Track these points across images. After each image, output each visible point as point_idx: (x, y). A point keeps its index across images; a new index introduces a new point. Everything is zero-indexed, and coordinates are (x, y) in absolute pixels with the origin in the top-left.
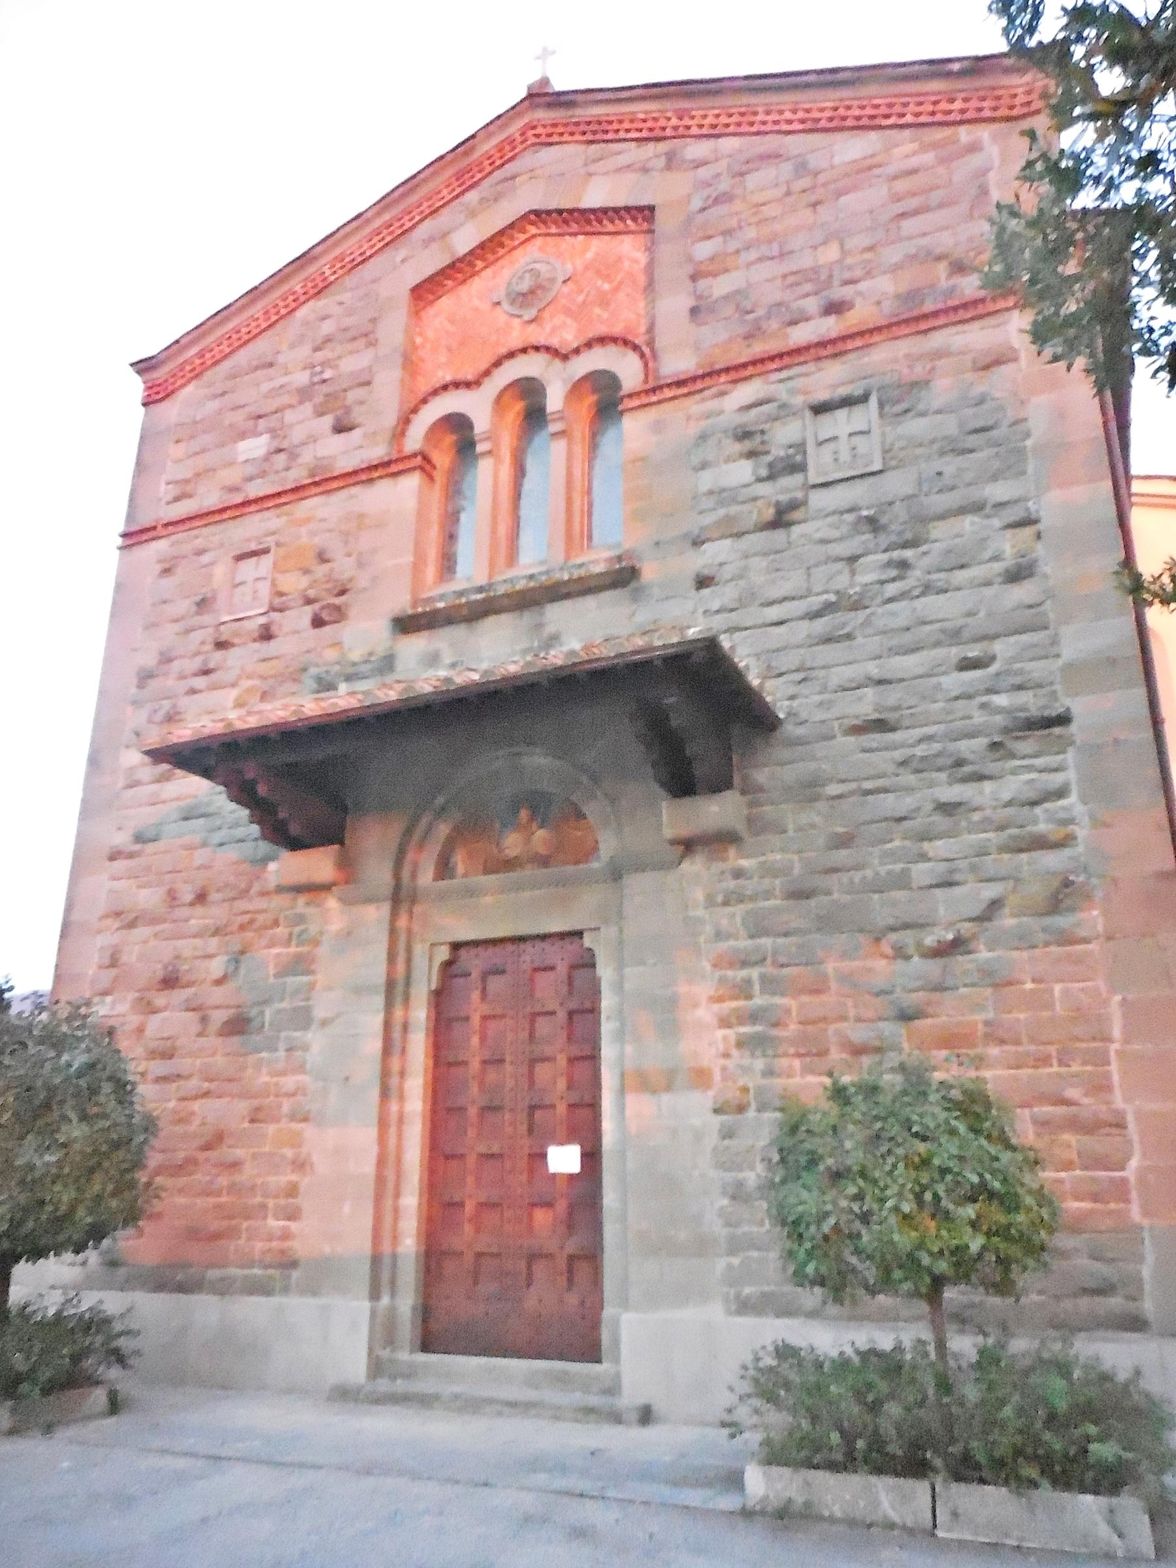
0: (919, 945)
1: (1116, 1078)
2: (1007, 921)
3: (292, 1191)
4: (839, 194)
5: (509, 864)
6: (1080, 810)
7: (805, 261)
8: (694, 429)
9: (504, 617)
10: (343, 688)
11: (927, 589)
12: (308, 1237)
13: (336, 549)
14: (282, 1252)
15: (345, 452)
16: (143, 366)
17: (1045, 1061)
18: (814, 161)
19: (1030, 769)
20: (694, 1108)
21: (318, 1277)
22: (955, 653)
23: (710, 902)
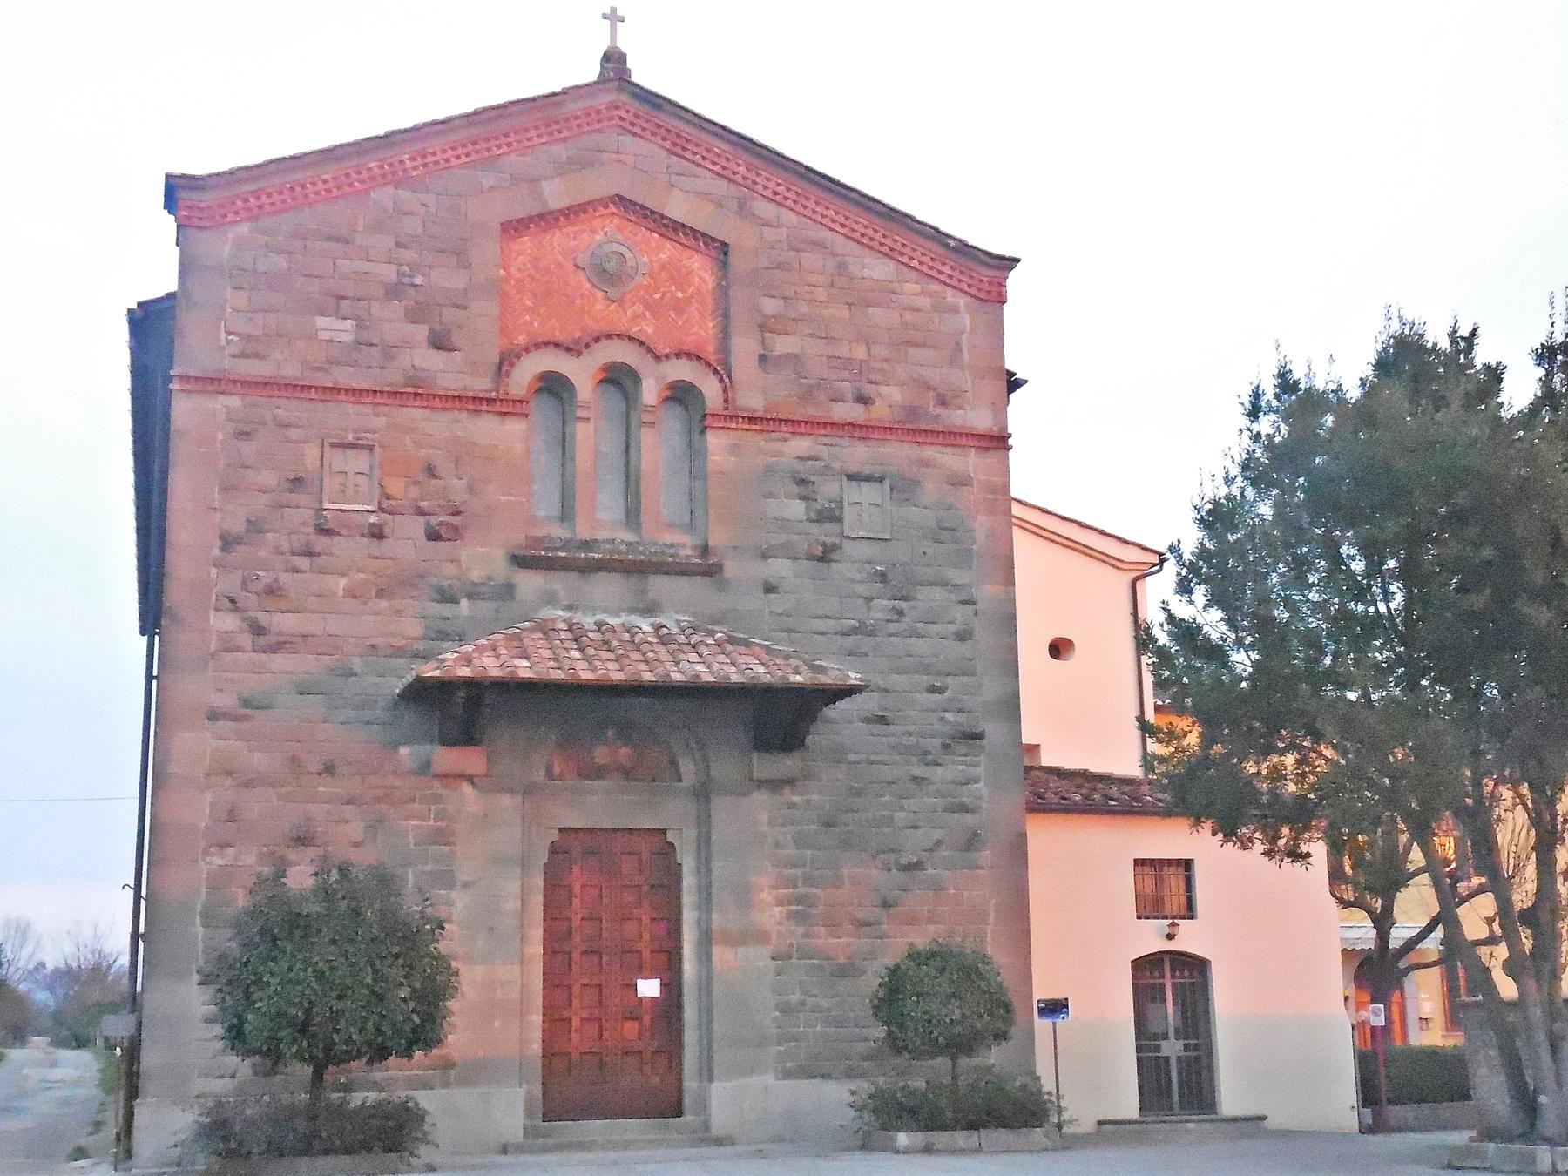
0: (897, 863)
5: (598, 773)
6: (985, 792)
7: (844, 351)
10: (464, 602)
13: (443, 465)
14: (441, 1057)
19: (962, 763)
20: (758, 957)
22: (925, 680)
23: (771, 823)
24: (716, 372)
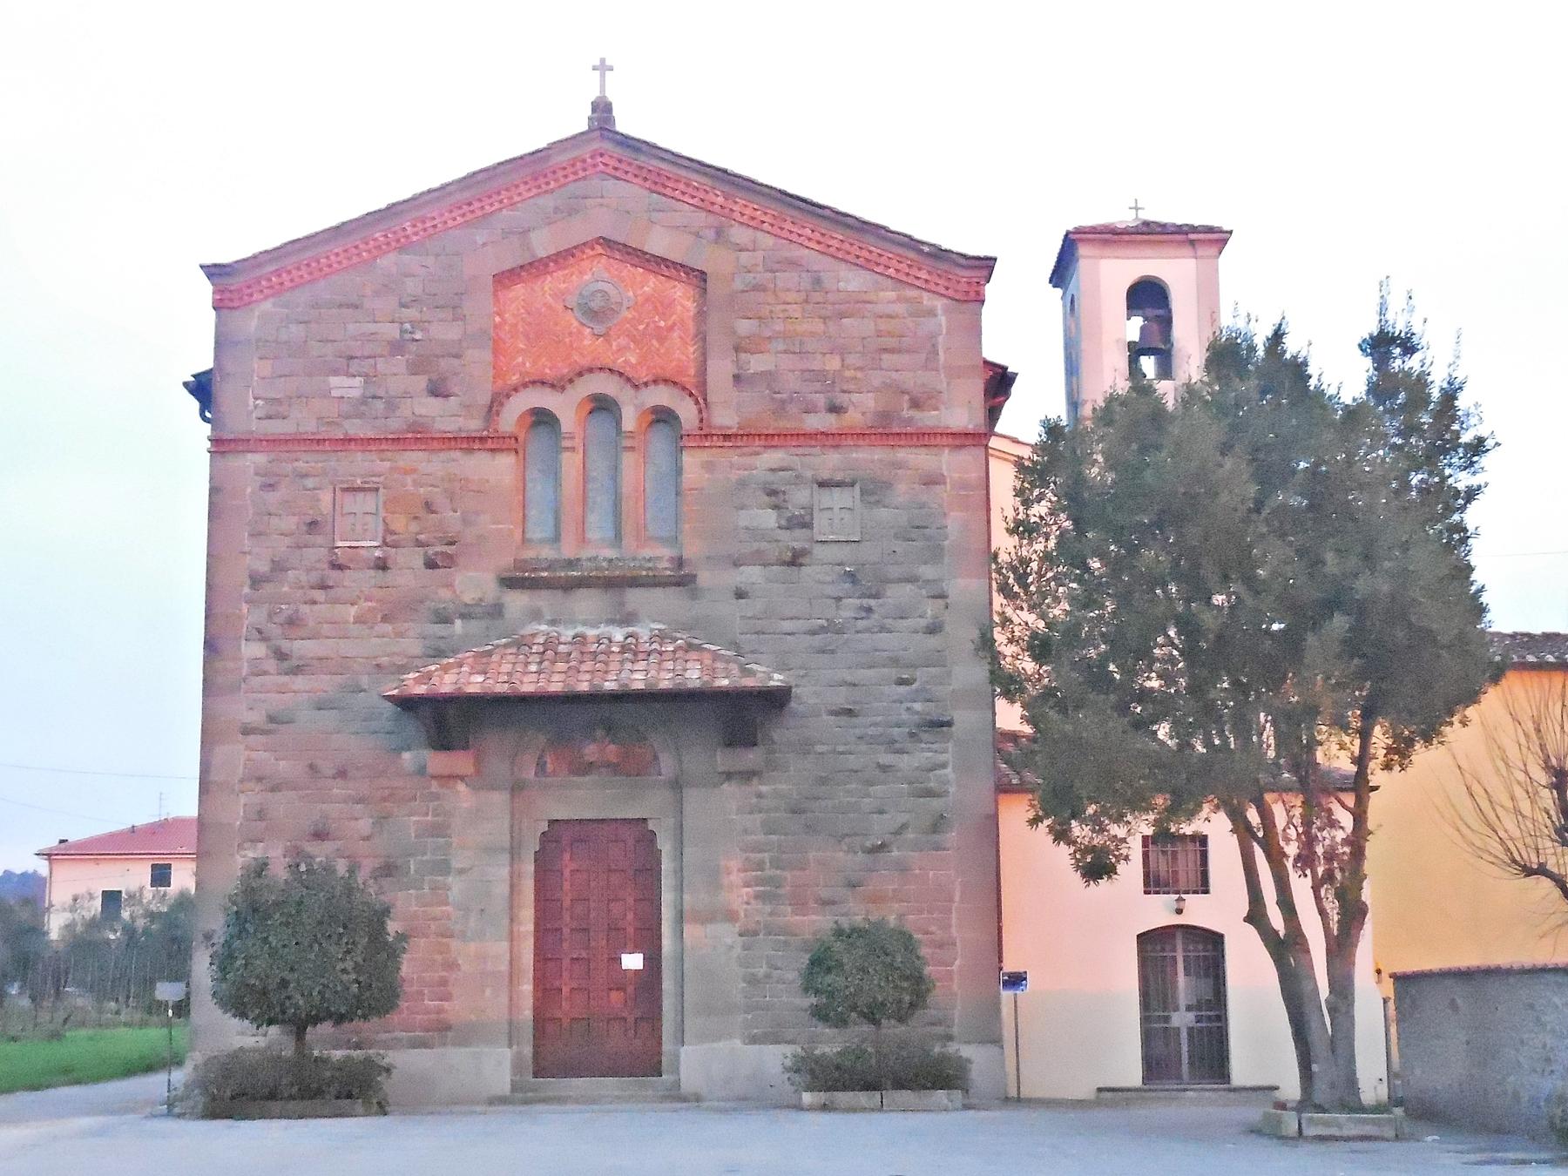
1: (954, 921)
2: (910, 835)
3: (444, 982)
4: (842, 316)
6: (952, 776)
7: (816, 365)
8: (734, 476)
9: (593, 591)
10: (458, 622)
11: (883, 629)
12: (457, 1009)
13: (440, 500)
15: (443, 416)
16: (214, 272)
17: (921, 912)
18: (828, 282)
19: (929, 750)
20: (727, 934)
21: (466, 1035)
22: (894, 673)
23: (739, 811)
24: (691, 395)
